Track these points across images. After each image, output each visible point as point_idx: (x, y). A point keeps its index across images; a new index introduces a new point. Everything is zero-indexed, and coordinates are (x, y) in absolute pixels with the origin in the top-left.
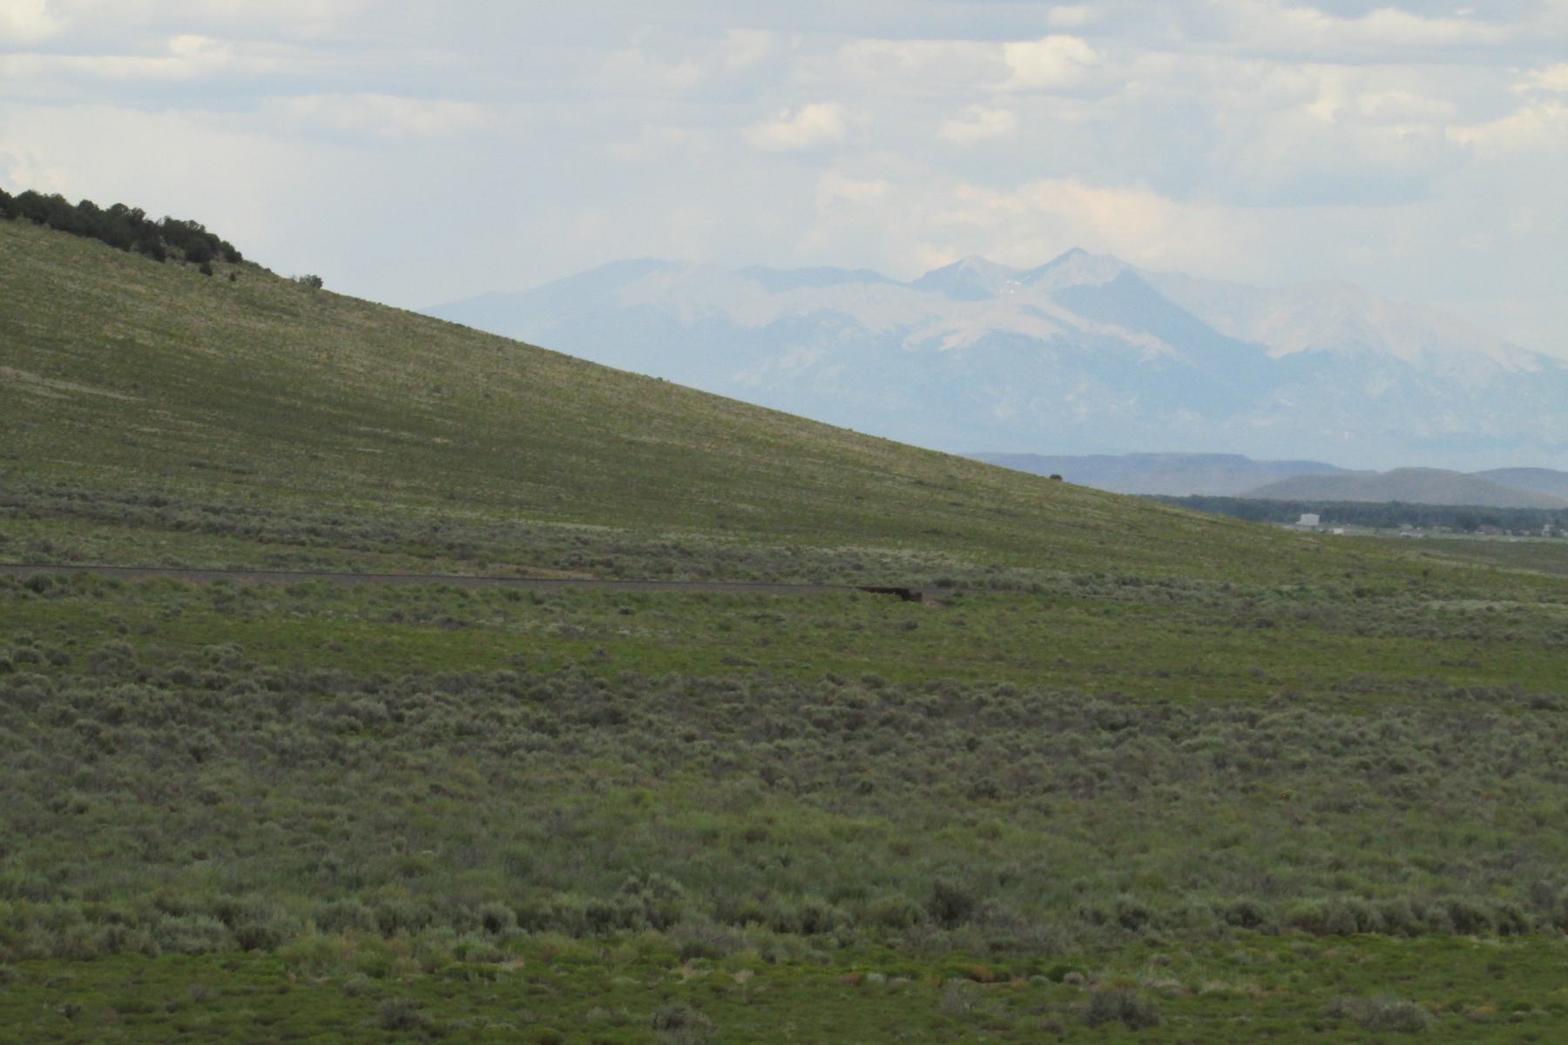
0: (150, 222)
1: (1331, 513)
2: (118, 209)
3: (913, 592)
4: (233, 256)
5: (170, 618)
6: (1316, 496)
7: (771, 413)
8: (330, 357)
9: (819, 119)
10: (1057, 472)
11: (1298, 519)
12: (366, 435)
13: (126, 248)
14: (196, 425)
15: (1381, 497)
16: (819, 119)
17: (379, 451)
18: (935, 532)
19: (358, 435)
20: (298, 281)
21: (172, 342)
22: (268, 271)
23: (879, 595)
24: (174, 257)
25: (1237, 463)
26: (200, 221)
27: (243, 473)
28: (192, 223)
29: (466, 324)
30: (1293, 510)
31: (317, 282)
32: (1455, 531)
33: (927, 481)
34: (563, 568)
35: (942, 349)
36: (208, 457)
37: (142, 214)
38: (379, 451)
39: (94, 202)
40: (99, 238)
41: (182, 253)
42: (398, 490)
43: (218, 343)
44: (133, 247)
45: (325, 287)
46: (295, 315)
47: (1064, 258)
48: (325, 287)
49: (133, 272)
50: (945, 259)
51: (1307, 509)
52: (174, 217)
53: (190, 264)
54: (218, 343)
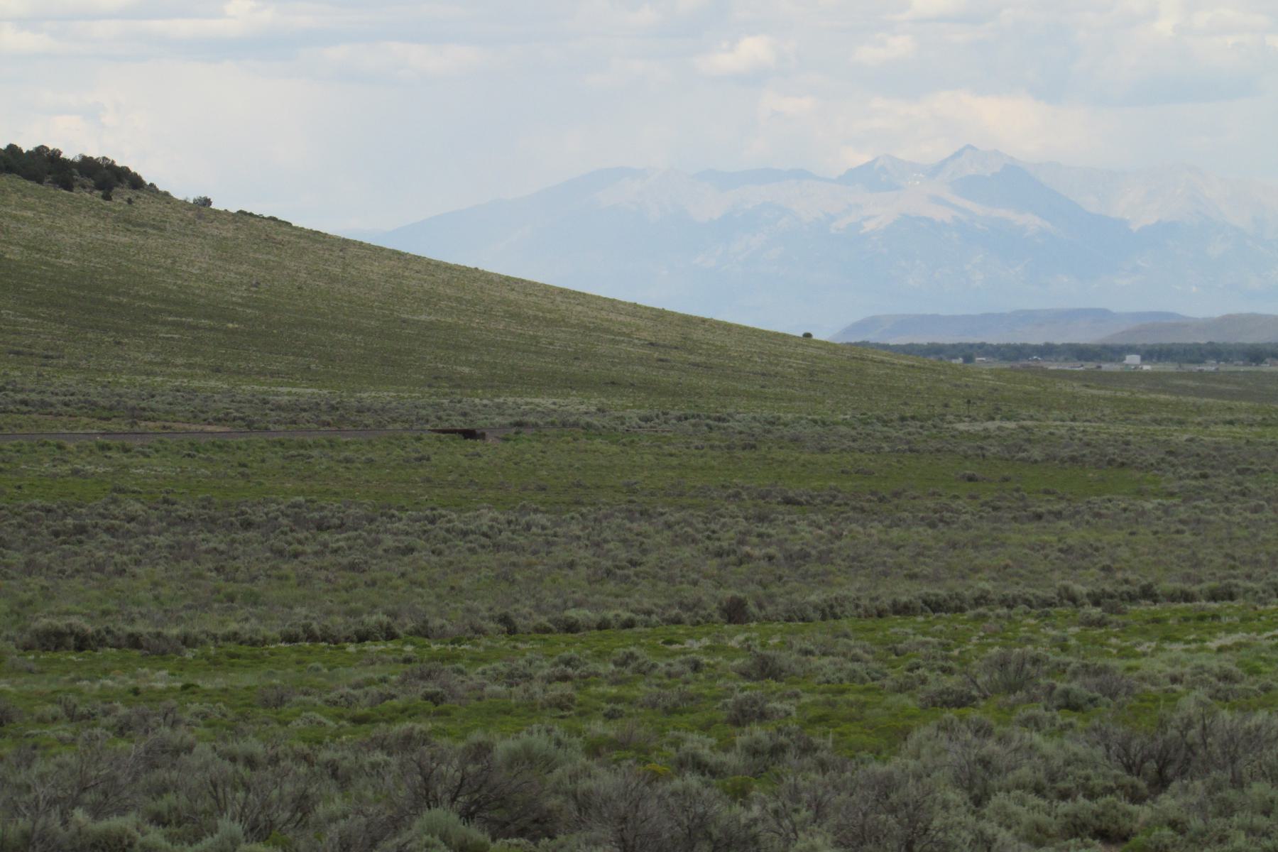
0: (65, 159)
1: (1150, 354)
2: (41, 150)
3: (478, 432)
4: (136, 182)
5: (1067, 465)
6: (1139, 341)
7: (563, 292)
8: (174, 262)
9: (754, 49)
10: (808, 331)
11: (1124, 359)
12: (173, 324)
13: (40, 182)
14: (31, 321)
15: (1202, 340)
16: (754, 49)
17: (176, 336)
18: (613, 383)
19: (164, 324)
20: (192, 202)
21: (38, 256)
22: (166, 194)
23: (443, 435)
24: (84, 187)
25: (1102, 315)
26: (111, 157)
27: (52, 357)
28: (104, 158)
29: (323, 231)
30: (1114, 352)
31: (207, 202)
32: (1245, 365)
33: (661, 342)
34: (209, 424)
35: (862, 232)
36: (30, 346)
37: (60, 153)
38: (176, 336)
39: (19, 146)
40: (18, 174)
41: (91, 183)
42: (176, 366)
43: (78, 255)
44: (47, 180)
45: (213, 206)
46: (161, 229)
47: (958, 154)
48: (213, 206)
49: (32, 200)
50: (865, 158)
51: (1131, 350)
52: (88, 155)
53: (96, 192)
54: (78, 255)
